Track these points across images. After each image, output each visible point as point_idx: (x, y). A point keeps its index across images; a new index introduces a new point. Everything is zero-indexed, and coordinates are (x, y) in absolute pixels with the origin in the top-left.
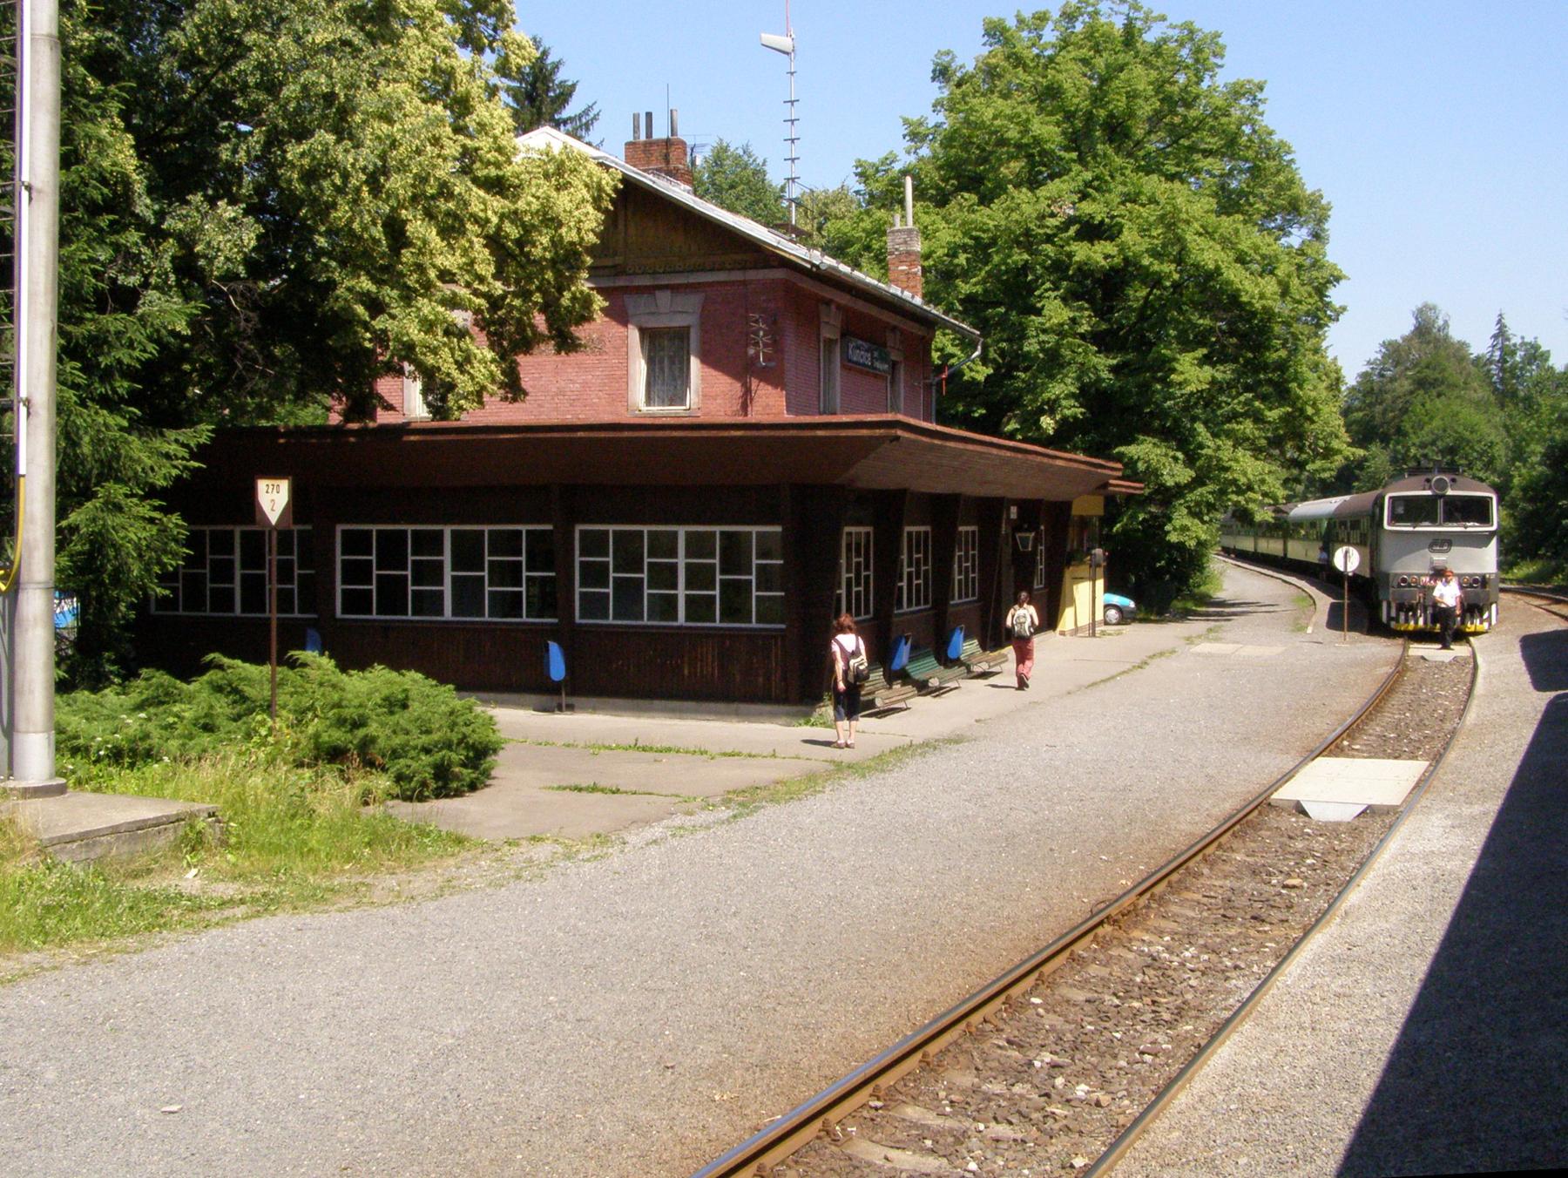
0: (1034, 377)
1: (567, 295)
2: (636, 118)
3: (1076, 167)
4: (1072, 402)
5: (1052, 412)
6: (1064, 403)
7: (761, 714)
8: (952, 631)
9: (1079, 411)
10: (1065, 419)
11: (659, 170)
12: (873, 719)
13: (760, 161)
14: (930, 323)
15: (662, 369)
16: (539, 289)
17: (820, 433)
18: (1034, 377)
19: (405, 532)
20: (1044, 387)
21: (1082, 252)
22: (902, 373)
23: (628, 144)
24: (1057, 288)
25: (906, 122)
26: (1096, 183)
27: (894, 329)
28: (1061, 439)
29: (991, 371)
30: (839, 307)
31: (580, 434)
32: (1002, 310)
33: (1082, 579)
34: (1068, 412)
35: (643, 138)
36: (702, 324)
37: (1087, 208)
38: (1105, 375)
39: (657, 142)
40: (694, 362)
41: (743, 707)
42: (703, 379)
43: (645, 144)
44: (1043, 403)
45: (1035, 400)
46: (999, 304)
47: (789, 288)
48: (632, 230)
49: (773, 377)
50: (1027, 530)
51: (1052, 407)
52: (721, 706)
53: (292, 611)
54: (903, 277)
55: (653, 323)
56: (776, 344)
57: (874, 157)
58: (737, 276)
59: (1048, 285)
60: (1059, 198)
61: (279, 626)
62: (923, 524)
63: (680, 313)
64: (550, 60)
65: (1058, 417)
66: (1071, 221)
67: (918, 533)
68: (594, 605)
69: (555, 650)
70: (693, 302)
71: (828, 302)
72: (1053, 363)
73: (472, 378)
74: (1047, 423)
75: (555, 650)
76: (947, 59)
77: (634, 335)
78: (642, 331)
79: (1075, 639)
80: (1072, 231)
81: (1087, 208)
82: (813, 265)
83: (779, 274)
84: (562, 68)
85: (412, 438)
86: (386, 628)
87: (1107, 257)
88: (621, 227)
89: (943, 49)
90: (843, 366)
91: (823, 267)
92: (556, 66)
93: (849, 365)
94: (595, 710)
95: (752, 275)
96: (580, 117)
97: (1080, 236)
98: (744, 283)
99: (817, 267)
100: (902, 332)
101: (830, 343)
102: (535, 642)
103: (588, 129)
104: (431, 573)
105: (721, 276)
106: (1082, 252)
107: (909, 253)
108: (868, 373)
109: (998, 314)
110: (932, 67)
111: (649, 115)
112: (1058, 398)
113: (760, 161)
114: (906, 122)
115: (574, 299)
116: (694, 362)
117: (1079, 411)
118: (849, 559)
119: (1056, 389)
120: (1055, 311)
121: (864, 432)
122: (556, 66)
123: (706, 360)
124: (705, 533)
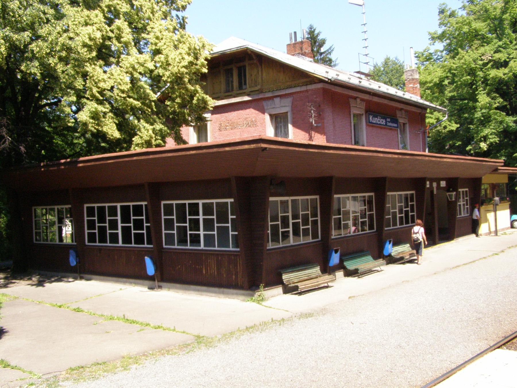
0: (477, 127)
1: (195, 98)
2: (291, 34)
3: (495, 41)
4: (494, 136)
5: (485, 141)
6: (490, 137)
7: (233, 294)
8: (385, 243)
9: (497, 140)
10: (491, 143)
11: (299, 54)
12: (297, 296)
13: (401, 62)
14: (424, 108)
15: (281, 131)
16: (180, 96)
17: (227, 149)
18: (477, 127)
19: (105, 207)
20: (482, 131)
21: (493, 73)
22: (407, 126)
23: (288, 45)
24: (484, 90)
25: (430, 34)
26: (504, 46)
27: (401, 109)
28: (492, 152)
29: (458, 126)
30: (362, 100)
31: (135, 158)
32: (466, 101)
33: (489, 211)
34: (491, 140)
35: (293, 42)
36: (292, 110)
37: (497, 56)
38: (512, 124)
39: (298, 43)
40: (290, 127)
41: (226, 290)
42: (294, 133)
43: (295, 44)
44: (481, 137)
45: (478, 136)
46: (465, 99)
47: (324, 90)
48: (264, 74)
49: (320, 130)
50: (452, 191)
51: (485, 139)
52: (217, 289)
53: (217, 223)
54: (411, 89)
55: (274, 112)
56: (320, 116)
57: (421, 50)
58: (304, 88)
59: (481, 89)
60: (487, 52)
61: (314, 217)
62: (413, 190)
63: (283, 106)
64: (316, 32)
65: (488, 143)
66: (490, 61)
67: (406, 195)
68: (170, 238)
69: (148, 261)
70: (288, 101)
71: (355, 98)
72: (486, 121)
73: (141, 137)
74: (484, 146)
75: (148, 261)
76: (444, 6)
77: (267, 117)
78: (271, 116)
79: (488, 237)
80: (489, 65)
81: (497, 56)
82: (329, 79)
83: (320, 86)
84: (321, 35)
85: (81, 165)
86: (100, 249)
87: (504, 74)
88: (260, 73)
89: (442, 3)
90: (367, 125)
91: (333, 80)
92: (318, 34)
93: (369, 124)
94: (169, 288)
95: (310, 87)
96: (328, 50)
97: (492, 67)
98: (307, 91)
99: (330, 80)
100: (406, 111)
101: (358, 116)
102: (141, 254)
103: (330, 54)
104: (114, 225)
105: (298, 89)
106: (493, 73)
107: (413, 79)
108: (385, 128)
109: (465, 103)
110: (438, 11)
111: (295, 33)
112: (487, 135)
113: (401, 62)
114: (430, 34)
115: (198, 99)
116: (290, 127)
117: (497, 140)
118: (463, 198)
119: (486, 131)
120: (483, 99)
121: (246, 147)
122: (318, 34)
123: (295, 125)
124: (97, 211)
